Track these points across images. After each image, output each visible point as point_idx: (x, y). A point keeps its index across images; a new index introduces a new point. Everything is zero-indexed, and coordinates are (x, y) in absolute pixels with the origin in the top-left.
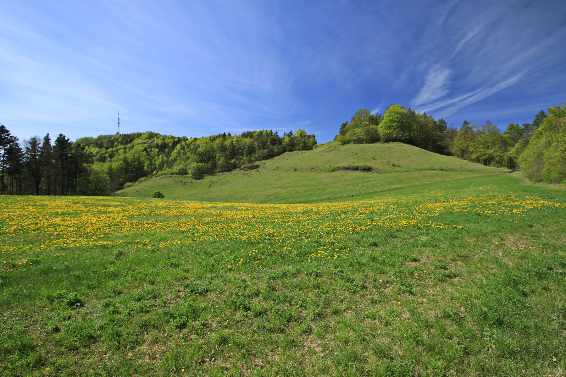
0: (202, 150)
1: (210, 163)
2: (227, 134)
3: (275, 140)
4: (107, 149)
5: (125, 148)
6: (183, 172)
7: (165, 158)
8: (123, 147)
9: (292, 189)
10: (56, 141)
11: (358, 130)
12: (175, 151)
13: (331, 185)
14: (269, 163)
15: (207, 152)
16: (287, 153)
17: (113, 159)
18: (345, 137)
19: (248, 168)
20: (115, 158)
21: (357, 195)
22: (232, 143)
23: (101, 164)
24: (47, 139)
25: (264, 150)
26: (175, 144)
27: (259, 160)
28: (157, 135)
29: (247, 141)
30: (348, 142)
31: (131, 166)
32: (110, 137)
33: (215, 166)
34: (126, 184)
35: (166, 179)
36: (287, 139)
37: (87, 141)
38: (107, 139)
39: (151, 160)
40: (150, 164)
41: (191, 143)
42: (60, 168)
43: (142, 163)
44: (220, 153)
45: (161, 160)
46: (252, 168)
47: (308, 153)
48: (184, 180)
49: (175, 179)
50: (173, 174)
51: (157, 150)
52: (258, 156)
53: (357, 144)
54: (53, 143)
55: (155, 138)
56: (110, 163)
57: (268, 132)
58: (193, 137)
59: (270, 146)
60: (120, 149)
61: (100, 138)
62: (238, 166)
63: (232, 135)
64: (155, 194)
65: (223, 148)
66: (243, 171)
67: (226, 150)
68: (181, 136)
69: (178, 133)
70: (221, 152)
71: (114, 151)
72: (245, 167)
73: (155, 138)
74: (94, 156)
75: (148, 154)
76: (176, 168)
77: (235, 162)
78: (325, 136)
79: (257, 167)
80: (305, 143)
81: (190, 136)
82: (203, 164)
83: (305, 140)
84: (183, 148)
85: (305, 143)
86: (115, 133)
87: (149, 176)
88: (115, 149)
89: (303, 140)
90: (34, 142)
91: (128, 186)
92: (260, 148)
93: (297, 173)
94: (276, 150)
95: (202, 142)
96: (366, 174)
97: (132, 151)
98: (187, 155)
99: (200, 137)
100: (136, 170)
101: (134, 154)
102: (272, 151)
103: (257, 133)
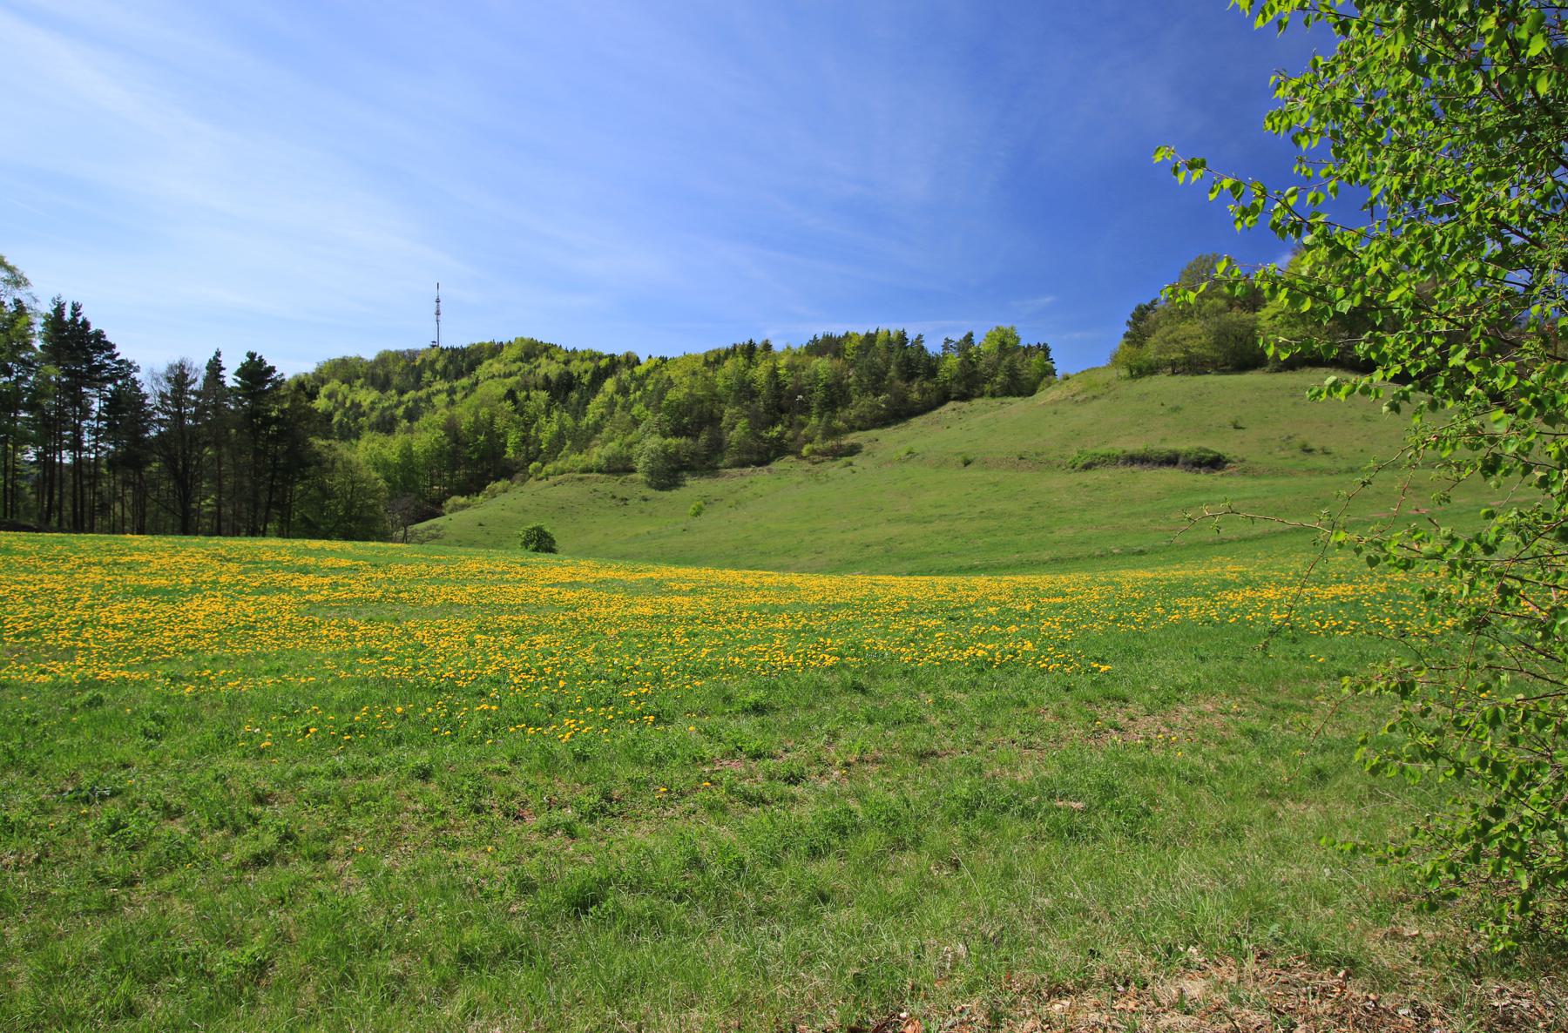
0: (680, 395)
1: (703, 438)
2: (758, 342)
3: (912, 362)
4: (402, 392)
5: (451, 392)
6: (620, 467)
7: (569, 422)
8: (447, 386)
9: (943, 525)
10: (238, 373)
11: (1186, 328)
12: (600, 398)
13: (1076, 516)
14: (892, 439)
15: (692, 404)
16: (951, 405)
17: (416, 424)
18: (1147, 349)
19: (824, 454)
20: (423, 421)
21: (1155, 550)
22: (774, 373)
23: (381, 438)
24: (215, 367)
25: (876, 395)
26: (599, 376)
27: (860, 429)
28: (547, 349)
29: (822, 365)
30: (1152, 370)
31: (466, 445)
32: (413, 355)
33: (717, 446)
34: (450, 502)
35: (567, 486)
36: (953, 360)
37: (346, 370)
38: (402, 363)
39: (528, 426)
40: (524, 440)
41: (648, 372)
42: (250, 456)
43: (499, 436)
44: (735, 404)
45: (555, 427)
46: (835, 454)
47: (1018, 404)
48: (622, 492)
49: (594, 486)
50: (588, 470)
51: (544, 395)
52: (858, 417)
53: (1178, 378)
54: (230, 380)
55: (543, 360)
56: (408, 437)
57: (893, 336)
58: (656, 355)
59: (893, 384)
60: (439, 392)
61: (383, 359)
62: (792, 447)
63: (778, 346)
64: (528, 533)
65: (745, 391)
66: (806, 465)
67: (753, 395)
68: (620, 352)
69: (612, 345)
70: (738, 402)
71: (421, 399)
72: (814, 452)
73: (543, 360)
74: (363, 415)
75: (519, 410)
76: (598, 453)
77: (782, 434)
78: (1082, 347)
79: (854, 450)
80: (1013, 374)
81: (646, 352)
82: (683, 440)
83: (1013, 362)
84: (623, 390)
85: (1011, 373)
86: (427, 345)
87: (519, 475)
88: (423, 393)
89: (1006, 362)
90: (179, 377)
91: (456, 508)
92: (865, 391)
93: (972, 473)
94: (916, 396)
95: (679, 373)
96: (1203, 478)
97: (473, 399)
98: (635, 411)
99: (678, 354)
100: (481, 458)
101: (477, 408)
102: (904, 400)
103: (855, 342)
